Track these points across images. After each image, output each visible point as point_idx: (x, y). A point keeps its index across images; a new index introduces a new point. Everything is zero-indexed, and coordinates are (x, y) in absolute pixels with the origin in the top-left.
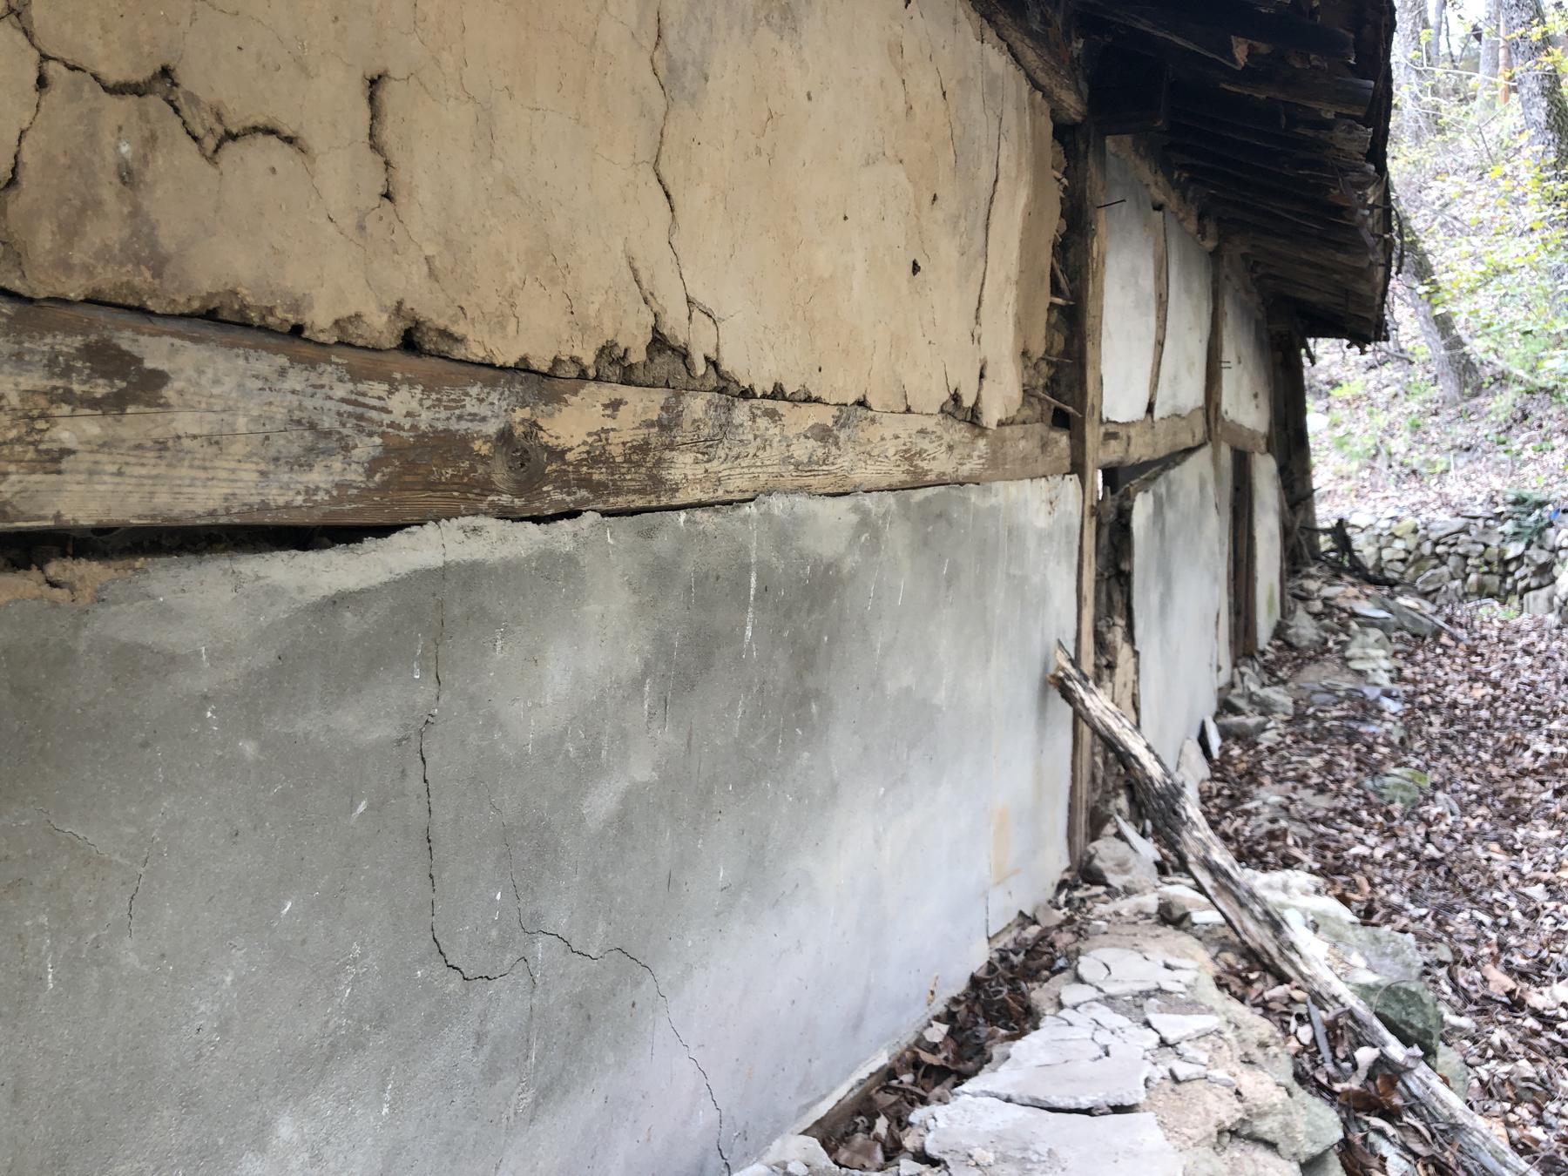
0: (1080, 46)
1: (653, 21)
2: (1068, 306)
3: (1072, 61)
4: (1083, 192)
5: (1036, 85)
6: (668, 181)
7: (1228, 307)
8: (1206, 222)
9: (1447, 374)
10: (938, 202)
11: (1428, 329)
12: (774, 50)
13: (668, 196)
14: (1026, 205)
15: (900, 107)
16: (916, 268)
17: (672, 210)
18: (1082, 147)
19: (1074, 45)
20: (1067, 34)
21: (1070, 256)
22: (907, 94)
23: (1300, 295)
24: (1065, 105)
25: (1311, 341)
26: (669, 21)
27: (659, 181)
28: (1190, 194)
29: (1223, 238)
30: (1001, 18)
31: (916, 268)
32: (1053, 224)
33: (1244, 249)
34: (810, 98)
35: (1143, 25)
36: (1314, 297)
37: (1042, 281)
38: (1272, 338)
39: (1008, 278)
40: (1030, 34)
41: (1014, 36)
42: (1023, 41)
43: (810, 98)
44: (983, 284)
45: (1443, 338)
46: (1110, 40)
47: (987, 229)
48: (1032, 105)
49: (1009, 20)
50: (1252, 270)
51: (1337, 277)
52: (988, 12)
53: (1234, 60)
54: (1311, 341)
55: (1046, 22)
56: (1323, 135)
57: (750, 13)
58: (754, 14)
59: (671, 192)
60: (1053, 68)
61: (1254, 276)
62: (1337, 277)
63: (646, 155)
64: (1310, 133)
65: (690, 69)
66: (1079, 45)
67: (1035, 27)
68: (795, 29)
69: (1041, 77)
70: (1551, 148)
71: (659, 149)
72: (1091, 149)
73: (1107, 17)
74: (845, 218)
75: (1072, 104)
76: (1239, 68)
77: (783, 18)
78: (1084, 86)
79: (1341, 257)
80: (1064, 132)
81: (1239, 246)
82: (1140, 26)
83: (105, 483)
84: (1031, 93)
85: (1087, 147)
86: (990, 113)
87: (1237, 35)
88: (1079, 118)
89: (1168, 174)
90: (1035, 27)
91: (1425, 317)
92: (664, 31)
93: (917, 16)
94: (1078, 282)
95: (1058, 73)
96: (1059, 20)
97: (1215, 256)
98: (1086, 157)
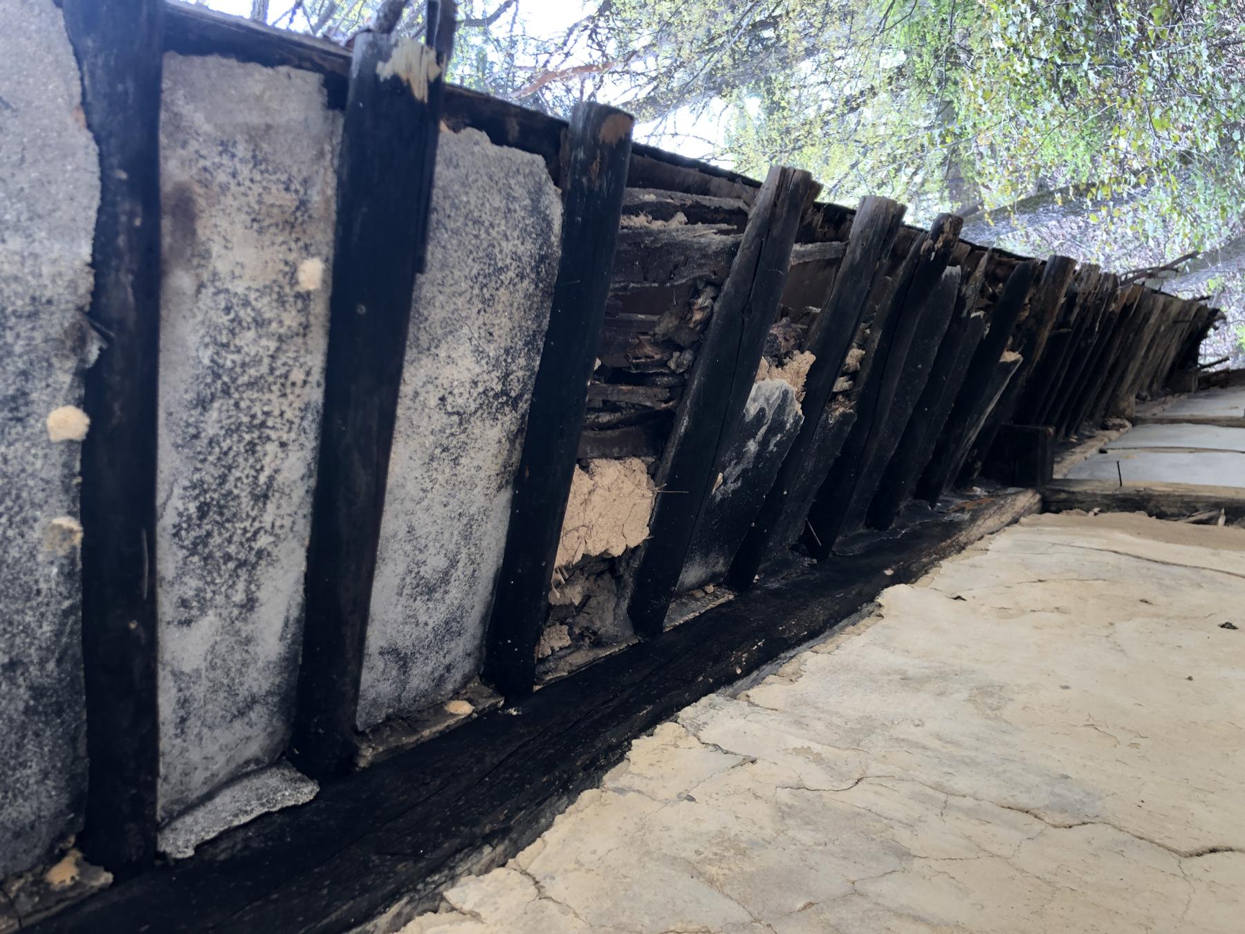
0: (979, 490)
1: (1013, 813)
2: (1226, 514)
3: (992, 496)
4: (1106, 496)
5: (1015, 521)
6: (1197, 846)
7: (1185, 413)
8: (1110, 424)
9: (1239, 261)
10: (1148, 598)
11: (1194, 279)
12: (1023, 709)
13: (1213, 851)
14: (1132, 535)
15: (1056, 617)
16: (1228, 626)
17: (1231, 850)
18: (1063, 496)
19: (978, 493)
20: (971, 498)
21: (1169, 511)
22: (1044, 610)
23: (1169, 364)
24: (1028, 504)
25: (1201, 361)
26: (1010, 799)
27: (1199, 855)
28: (1087, 433)
29: (1120, 414)
30: (962, 539)
31: (1228, 626)
32: (1140, 517)
33: (1133, 399)
34: (1067, 687)
35: (973, 436)
36: (1172, 353)
37: (1205, 530)
38: (1203, 389)
39: (1213, 554)
40: (973, 520)
41: (975, 531)
42: (979, 526)
43: (1067, 687)
44: (1228, 573)
45: (1206, 266)
46: (980, 464)
47: (1168, 564)
48: (1030, 525)
49: (964, 532)
50: (1144, 399)
51: (1162, 328)
52: (957, 547)
53: (1015, 362)
54: (1201, 361)
55: (962, 510)
56: (1079, 300)
57: (990, 722)
58: (990, 719)
59: (1211, 845)
60: (1000, 509)
61: (1149, 398)
62: (1162, 328)
63: (1173, 860)
64: (1076, 311)
65: (1058, 790)
66: (978, 491)
67: (967, 516)
68: (1001, 688)
69: (1007, 518)
70: (1050, 208)
71: (1159, 845)
72: (1066, 488)
73: (961, 464)
74: (1190, 678)
75: (1027, 499)
76: (1022, 359)
77: (992, 695)
78: (1011, 490)
79: (1152, 320)
80: (1047, 506)
81: (1129, 403)
82: (973, 438)
84: (1021, 525)
85: (1064, 491)
86: (1051, 551)
87: (999, 358)
88: (1038, 496)
89: (1074, 445)
90: (967, 516)
91: (1182, 283)
92: (1021, 806)
93: (972, 593)
94: (1199, 505)
95: (1003, 506)
96: (959, 501)
97: (1135, 422)
98: (1073, 493)
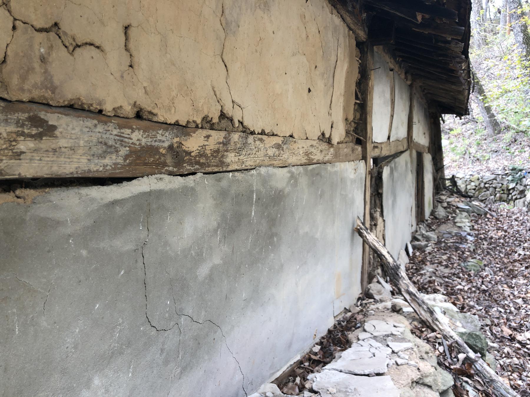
0: (365, 15)
1: (221, 7)
2: (361, 103)
3: (362, 21)
4: (366, 65)
5: (350, 29)
6: (226, 61)
7: (415, 104)
8: (408, 75)
9: (489, 126)
10: (317, 68)
11: (483, 111)
12: (261, 17)
13: (226, 66)
14: (347, 69)
15: (304, 36)
16: (309, 90)
17: (227, 71)
18: (366, 50)
19: (363, 15)
20: (361, 11)
21: (362, 86)
22: (306, 32)
23: (439, 100)
24: (360, 35)
25: (443, 115)
26: (226, 7)
27: (223, 61)
28: (402, 65)
29: (413, 80)
30: (338, 6)
31: (309, 90)
32: (356, 76)
33: (421, 84)
34: (274, 33)
35: (386, 9)
36: (444, 100)
37: (352, 95)
38: (430, 114)
39: (341, 94)
40: (348, 11)
41: (343, 12)
42: (346, 14)
43: (274, 33)
44: (332, 96)
45: (488, 114)
46: (375, 13)
47: (334, 77)
48: (349, 36)
49: (341, 7)
50: (423, 91)
51: (452, 93)
52: (334, 4)
53: (417, 20)
54: (443, 115)
55: (354, 7)
56: (447, 46)
57: (254, 4)
58: (255, 5)
59: (227, 65)
60: (356, 23)
61: (424, 93)
62: (452, 93)
63: (219, 52)
64: (443, 45)
65: (233, 23)
66: (365, 15)
67: (350, 9)
68: (269, 10)
69: (352, 26)
70: (524, 50)
71: (223, 50)
72: (369, 50)
73: (374, 6)
74: (286, 74)
75: (362, 35)
76: (419, 23)
77: (265, 6)
78: (366, 29)
79: (453, 87)
80: (360, 45)
81: (419, 83)
82: (385, 9)
84: (348, 31)
85: (368, 50)
86: (335, 38)
87: (418, 12)
88: (365, 40)
89: (395, 59)
90: (350, 9)
91: (482, 107)
92: (225, 11)
93: (310, 5)
94: (364, 95)
95: (357, 25)
96: (358, 7)
97: (411, 86)
98: (367, 53)
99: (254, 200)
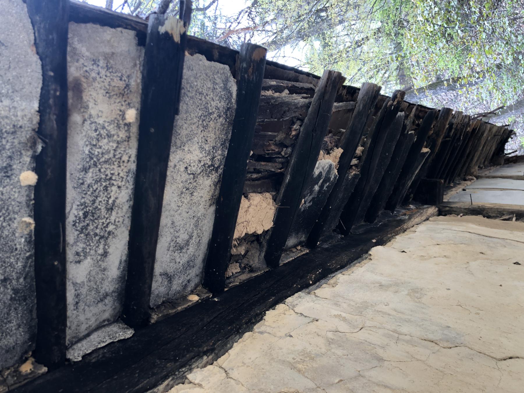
0: (412, 206)
1: (426, 342)
2: (516, 216)
3: (418, 209)
4: (465, 209)
5: (427, 219)
6: (504, 356)
7: (499, 174)
8: (467, 178)
9: (522, 110)
10: (483, 252)
11: (503, 117)
12: (431, 298)
13: (511, 358)
14: (476, 225)
15: (445, 259)
16: (517, 263)
17: (518, 358)
18: (447, 209)
19: (412, 207)
20: (409, 209)
21: (492, 215)
22: (439, 257)
23: (492, 153)
24: (432, 212)
25: (506, 152)
26: (425, 336)
27: (505, 360)
28: (458, 182)
29: (471, 174)
30: (405, 227)
31: (517, 263)
32: (480, 218)
33: (477, 168)
34: (449, 289)
35: (410, 183)
36: (493, 149)
37: (507, 223)
38: (507, 164)
39: (511, 233)
40: (410, 219)
41: (410, 224)
42: (412, 221)
43: (449, 289)
44: (517, 241)
45: (507, 112)
46: (412, 195)
47: (491, 237)
48: (434, 221)
49: (406, 224)
50: (481, 168)
51: (489, 138)
52: (403, 230)
53: (427, 153)
54: (506, 152)
55: (405, 215)
56: (454, 126)
57: (417, 304)
58: (417, 302)
59: (510, 356)
60: (421, 214)
61: (483, 168)
62: (489, 138)
63: (494, 362)
64: (453, 131)
65: (445, 332)
66: (412, 206)
67: (407, 217)
68: (421, 289)
69: (424, 218)
70: (442, 87)
71: (488, 356)
72: (449, 206)
73: (405, 195)
74: (501, 285)
75: (432, 210)
76: (430, 151)
77: (417, 292)
78: (425, 206)
79: (485, 135)
80: (441, 213)
81: (475, 169)
82: (410, 184)
83: (94, 358)
84: (430, 221)
85: (448, 207)
86: (442, 232)
87: (421, 151)
88: (437, 209)
89: (452, 187)
90: (407, 217)
91: (497, 119)
92: (430, 339)
93: (409, 250)
94: (505, 213)
95: (422, 213)
96: (404, 211)
97: (478, 177)
98: (452, 207)
99: (137, 388)
